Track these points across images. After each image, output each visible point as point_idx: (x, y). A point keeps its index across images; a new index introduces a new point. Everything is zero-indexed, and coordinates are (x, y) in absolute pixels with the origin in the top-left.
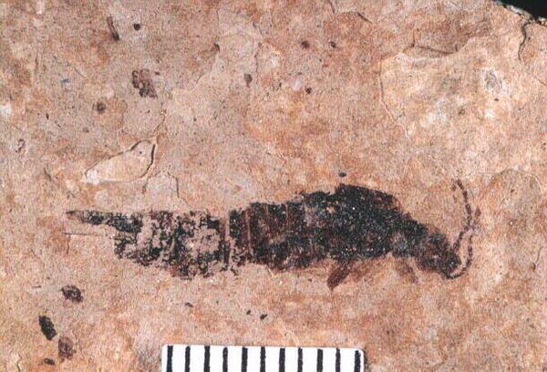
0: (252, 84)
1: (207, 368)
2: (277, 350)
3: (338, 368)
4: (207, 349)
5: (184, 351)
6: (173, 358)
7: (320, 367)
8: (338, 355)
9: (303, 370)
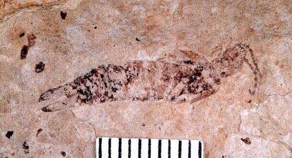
1: (120, 156)
2: (157, 141)
3: (190, 156)
4: (120, 140)
5: (108, 140)
6: (102, 145)
7: (120, 156)
8: (190, 144)
9: (182, 157)
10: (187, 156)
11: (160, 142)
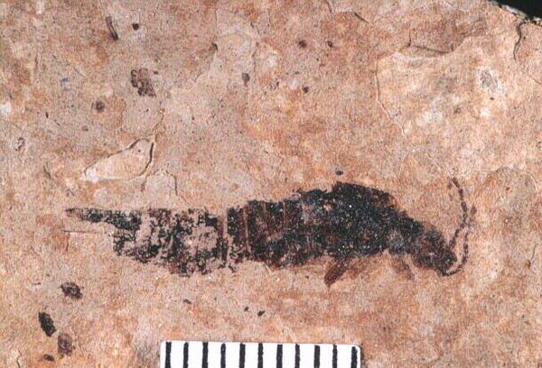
2: (275, 346)
4: (205, 345)
5: (183, 347)
8: (335, 351)
10: (274, 364)
11: (280, 349)
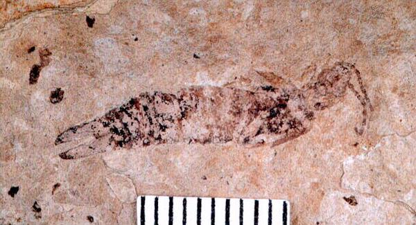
0: (73, 152)
1: (171, 222)
2: (224, 201)
3: (270, 222)
4: (171, 199)
5: (154, 200)
6: (145, 206)
7: (171, 222)
8: (270, 204)
9: (259, 224)
